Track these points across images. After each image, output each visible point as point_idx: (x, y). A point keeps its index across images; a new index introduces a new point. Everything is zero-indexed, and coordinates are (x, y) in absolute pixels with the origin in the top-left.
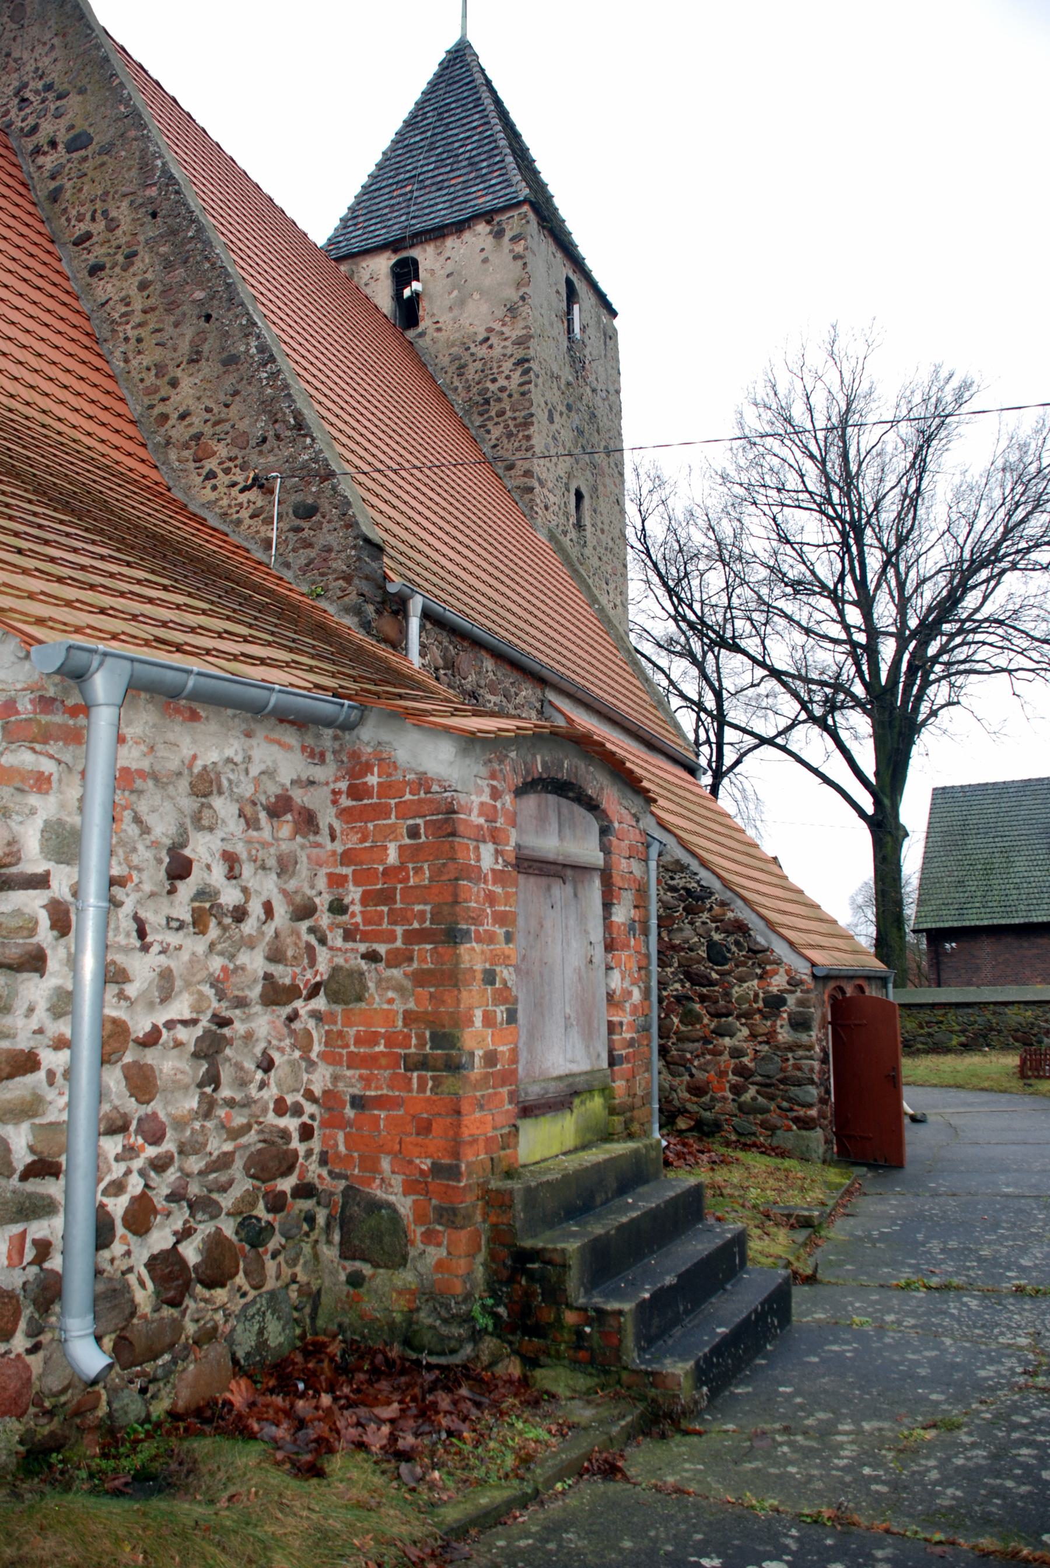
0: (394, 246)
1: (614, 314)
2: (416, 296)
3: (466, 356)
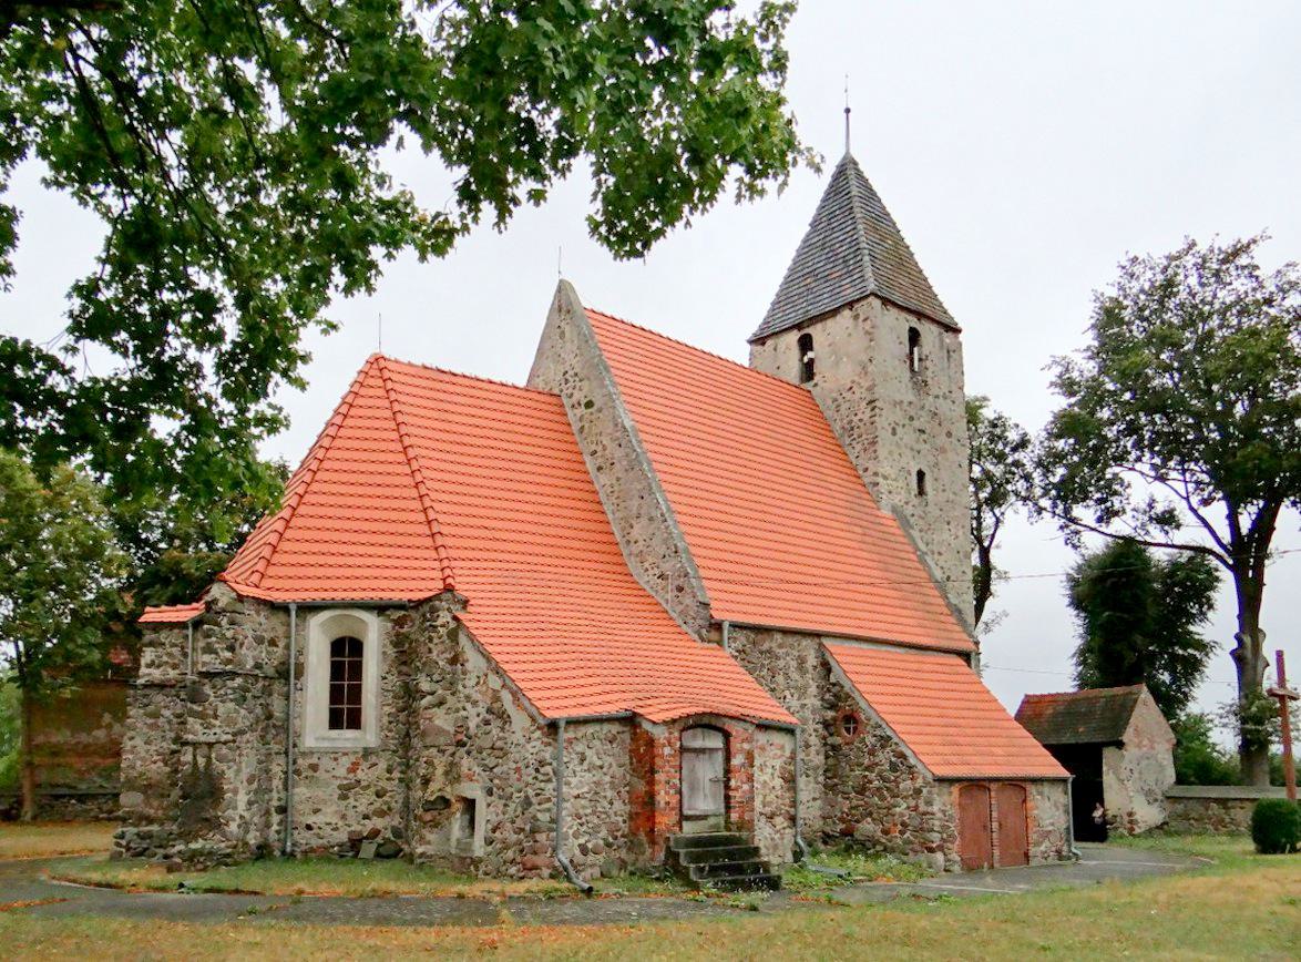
0: (799, 326)
1: (957, 331)
2: (811, 361)
3: (840, 398)
